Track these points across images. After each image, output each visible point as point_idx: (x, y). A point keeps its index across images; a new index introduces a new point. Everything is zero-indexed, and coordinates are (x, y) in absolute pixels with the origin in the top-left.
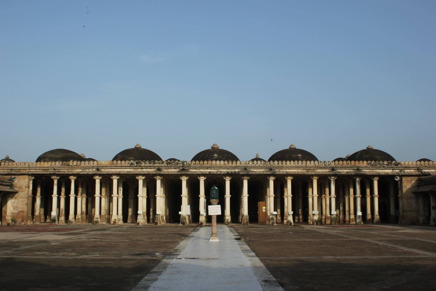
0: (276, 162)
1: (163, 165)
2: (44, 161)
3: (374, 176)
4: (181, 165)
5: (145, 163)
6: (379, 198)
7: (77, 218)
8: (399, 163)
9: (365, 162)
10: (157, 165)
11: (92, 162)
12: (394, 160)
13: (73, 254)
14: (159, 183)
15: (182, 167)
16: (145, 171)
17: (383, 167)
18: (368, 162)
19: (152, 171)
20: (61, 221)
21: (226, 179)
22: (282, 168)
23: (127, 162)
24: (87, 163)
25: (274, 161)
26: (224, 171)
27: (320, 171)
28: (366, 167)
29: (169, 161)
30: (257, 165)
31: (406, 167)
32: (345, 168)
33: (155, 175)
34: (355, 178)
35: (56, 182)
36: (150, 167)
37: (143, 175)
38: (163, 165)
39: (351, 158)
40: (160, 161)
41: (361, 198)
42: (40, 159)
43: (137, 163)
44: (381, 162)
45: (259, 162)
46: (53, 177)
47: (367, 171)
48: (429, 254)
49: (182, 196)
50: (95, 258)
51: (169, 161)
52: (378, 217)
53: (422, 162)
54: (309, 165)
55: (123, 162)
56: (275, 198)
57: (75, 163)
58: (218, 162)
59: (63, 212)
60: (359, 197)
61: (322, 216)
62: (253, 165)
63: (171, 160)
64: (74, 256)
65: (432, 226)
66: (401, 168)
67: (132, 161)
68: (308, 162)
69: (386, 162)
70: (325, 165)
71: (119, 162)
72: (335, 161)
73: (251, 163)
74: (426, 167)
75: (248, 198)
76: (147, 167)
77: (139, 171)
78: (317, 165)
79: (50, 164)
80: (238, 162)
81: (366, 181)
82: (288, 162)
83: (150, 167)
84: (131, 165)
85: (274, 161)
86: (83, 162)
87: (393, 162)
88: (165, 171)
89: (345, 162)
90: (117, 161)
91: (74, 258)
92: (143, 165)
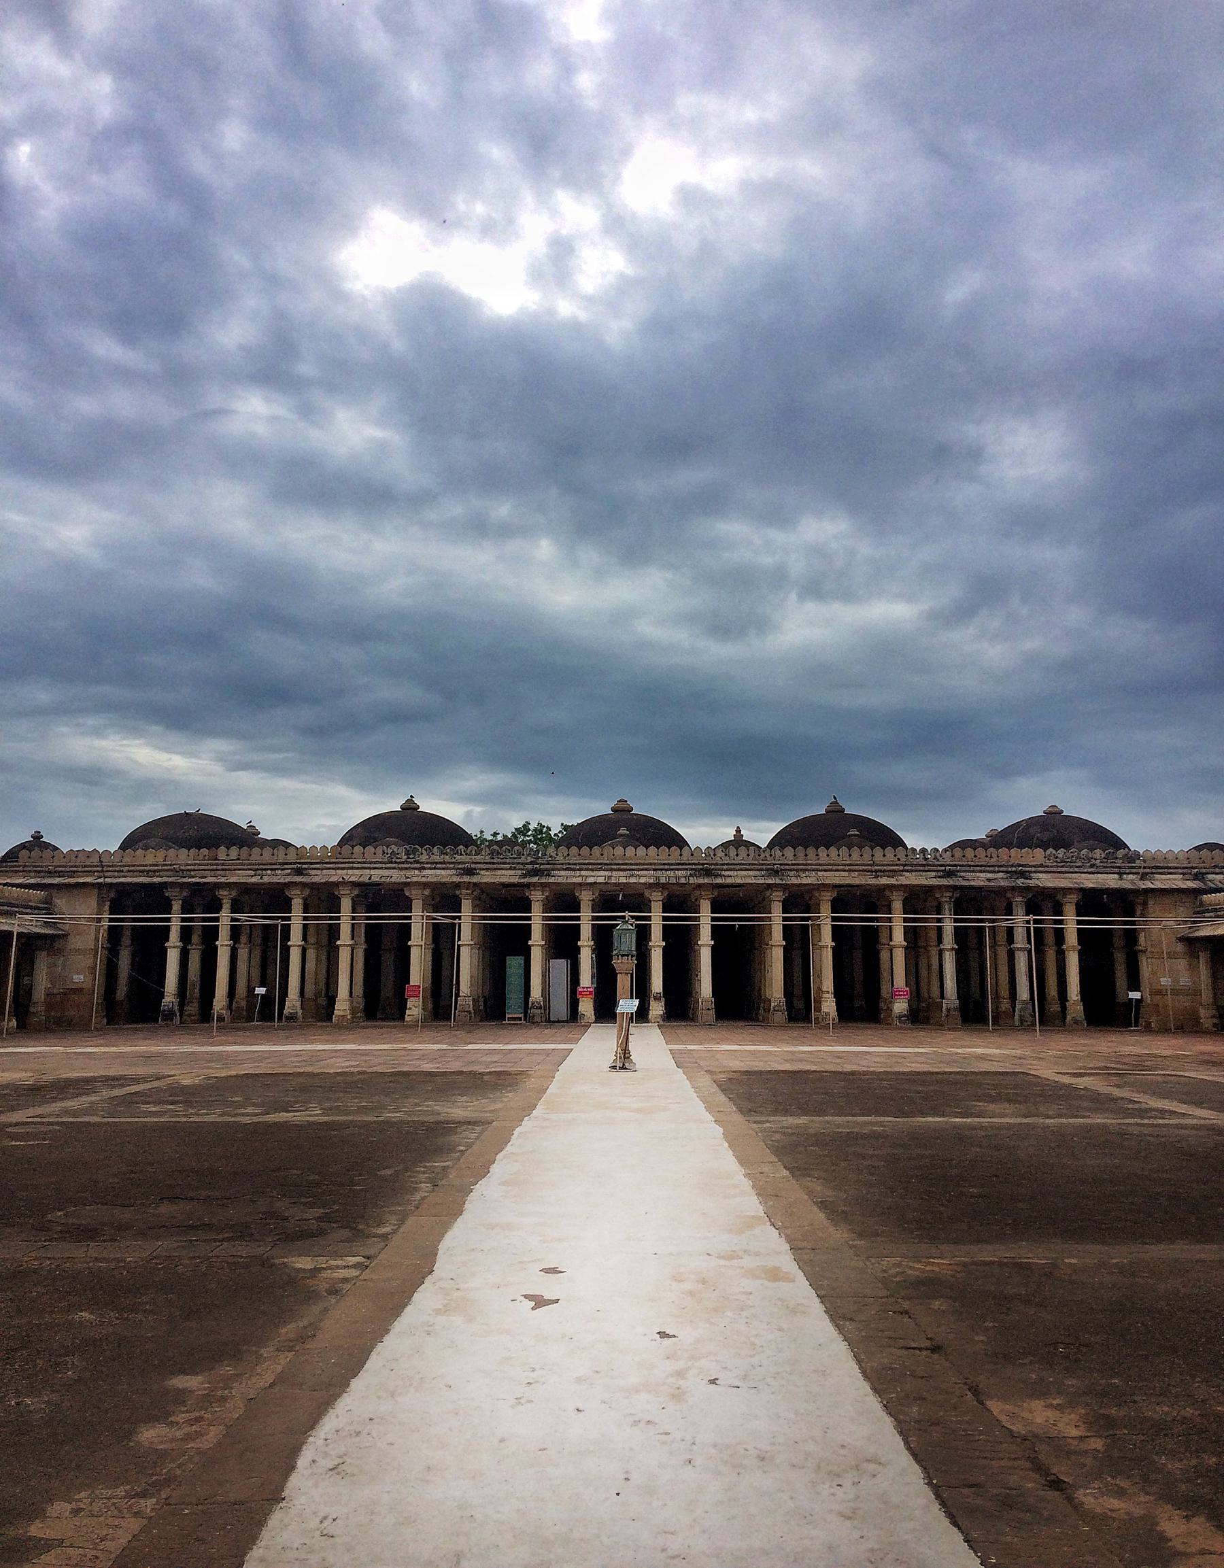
0: (789, 851)
1: (479, 858)
2: (146, 848)
3: (1065, 891)
4: (530, 859)
5: (430, 852)
6: (1081, 953)
7: (235, 1005)
8: (1137, 855)
9: (1039, 852)
10: (464, 858)
12: (1124, 846)
13: (250, 1110)
15: (531, 863)
16: (432, 875)
17: (1092, 866)
18: (1048, 852)
19: (446, 875)
20: (189, 1015)
21: (532, 898)
22: (805, 868)
23: (379, 850)
24: (267, 852)
25: (782, 848)
26: (646, 878)
28: (1041, 866)
29: (495, 847)
31: (1158, 867)
32: (984, 868)
33: (458, 886)
34: (1009, 895)
36: (444, 865)
37: (425, 885)
38: (479, 858)
39: (1000, 840)
40: (473, 848)
41: (957, 952)
42: (129, 843)
43: (407, 854)
44: (1084, 852)
45: (743, 851)
46: (222, 893)
47: (1045, 880)
48: (1204, 1115)
49: (530, 943)
50: (312, 1119)
51: (495, 847)
52: (1080, 1008)
53: (1205, 852)
54: (882, 858)
55: (370, 849)
56: (787, 950)
57: (234, 852)
58: (630, 851)
59: (195, 992)
60: (953, 949)
61: (919, 1001)
64: (256, 1115)
65: (1207, 1032)
66: (1141, 871)
68: (878, 852)
69: (1098, 854)
70: (926, 859)
71: (359, 849)
72: (952, 847)
73: (720, 854)
74: (1215, 867)
75: (665, 949)
76: (434, 865)
77: (416, 876)
78: (903, 859)
79: (161, 854)
80: (685, 851)
81: (1042, 902)
82: (822, 852)
83: (444, 863)
84: (391, 862)
85: (782, 848)
86: (256, 851)
87: (1121, 853)
88: (486, 877)
89: (981, 852)
90: (353, 847)
91: (255, 1119)
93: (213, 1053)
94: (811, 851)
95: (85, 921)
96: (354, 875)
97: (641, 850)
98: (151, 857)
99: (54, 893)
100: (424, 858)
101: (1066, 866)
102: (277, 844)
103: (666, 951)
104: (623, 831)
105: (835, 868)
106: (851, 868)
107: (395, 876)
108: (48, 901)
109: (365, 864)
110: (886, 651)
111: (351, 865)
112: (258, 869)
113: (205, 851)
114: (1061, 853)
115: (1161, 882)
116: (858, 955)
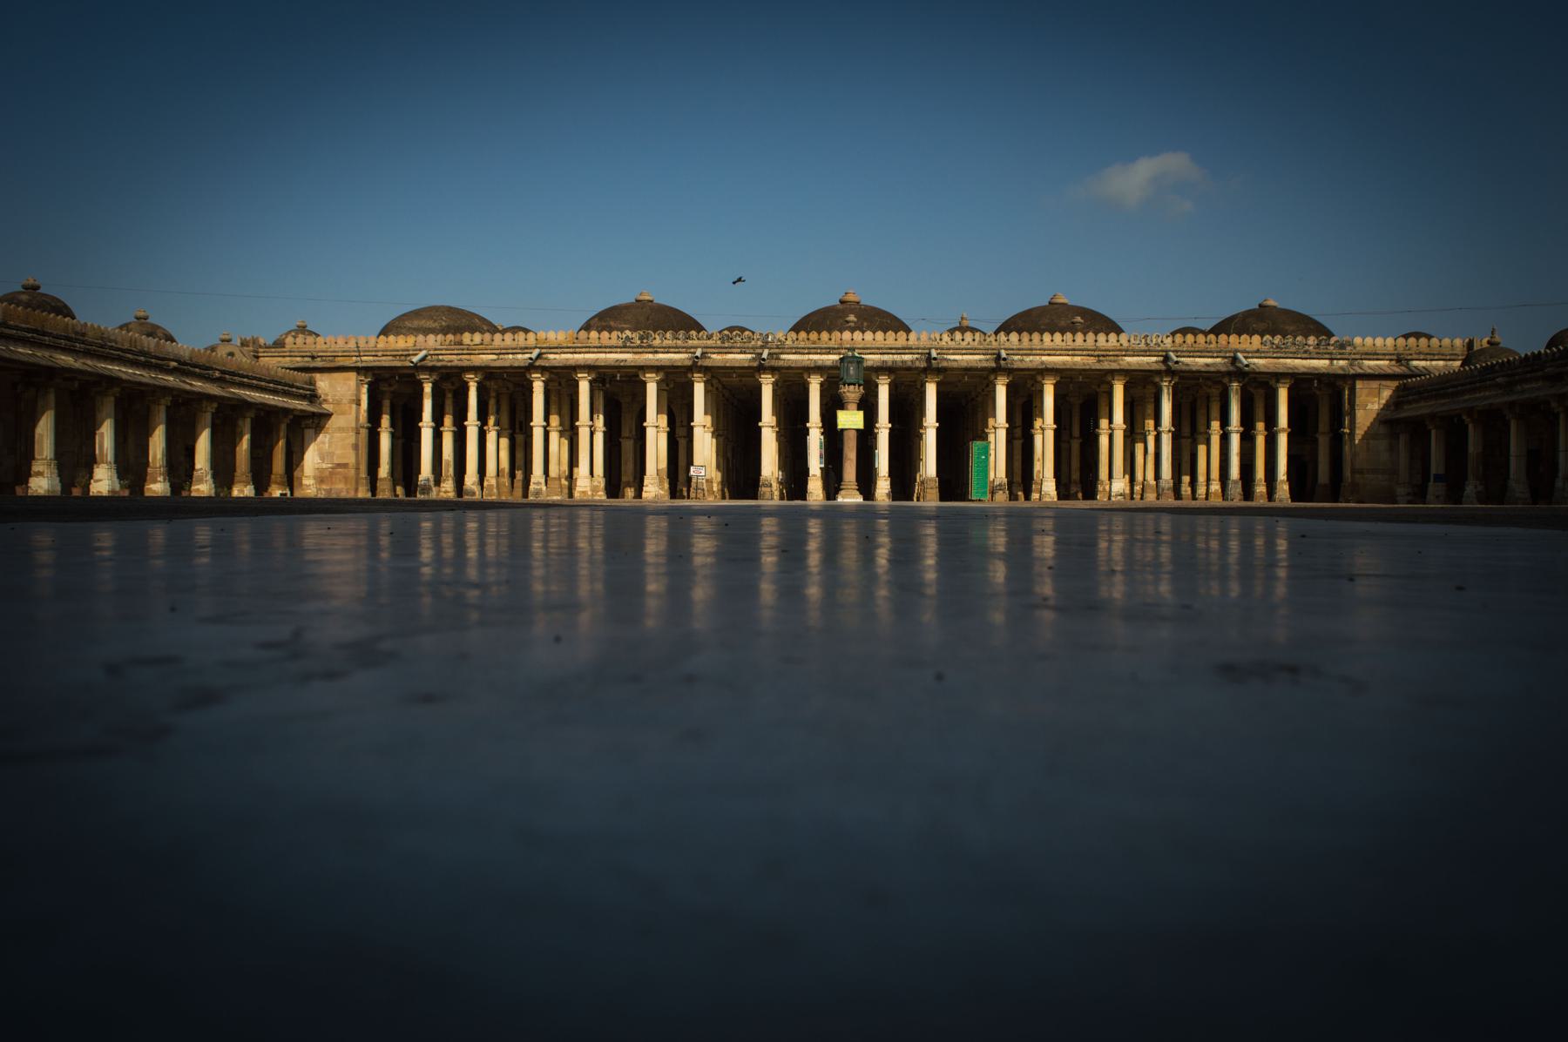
1: (710, 342)
3: (1278, 376)
11: (521, 335)
14: (699, 390)
16: (663, 357)
22: (1031, 351)
23: (615, 334)
24: (508, 336)
25: (1008, 334)
27: (1132, 361)
30: (964, 344)
32: (1202, 353)
35: (428, 388)
38: (710, 342)
43: (641, 338)
44: (1299, 338)
45: (968, 336)
47: (1260, 363)
52: (1286, 487)
57: (477, 338)
58: (858, 335)
62: (952, 344)
63: (731, 329)
67: (628, 333)
69: (1312, 340)
81: (1258, 389)
86: (498, 336)
88: (717, 359)
89: (1201, 338)
92: (657, 342)
93: (805, 417)
94: (1025, 336)
95: (343, 396)
96: (590, 357)
97: (869, 335)
98: (400, 342)
99: (318, 376)
100: (657, 342)
101: (1279, 352)
102: (515, 330)
103: (892, 431)
104: (852, 318)
105: (1057, 351)
106: (1072, 351)
107: (628, 357)
108: (312, 383)
109: (601, 348)
110: (1342, 368)
111: (588, 349)
112: (501, 352)
113: (450, 337)
114: (1277, 339)
115: (1370, 364)
116: (1076, 445)
